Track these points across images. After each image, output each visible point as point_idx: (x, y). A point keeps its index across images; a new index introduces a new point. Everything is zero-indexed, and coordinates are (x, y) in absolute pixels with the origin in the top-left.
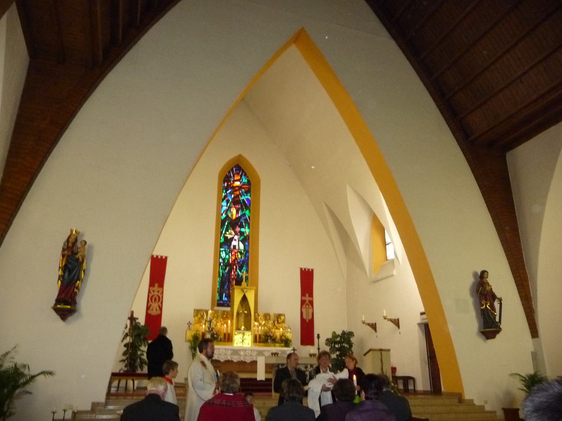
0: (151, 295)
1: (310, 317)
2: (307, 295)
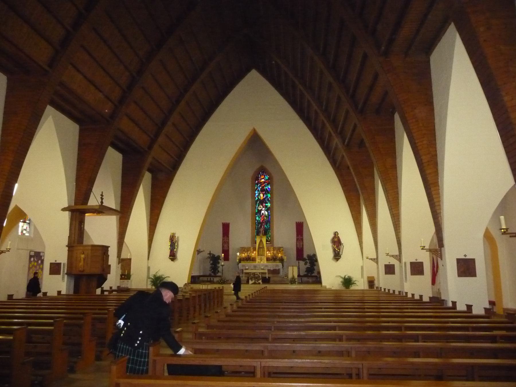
0: (224, 241)
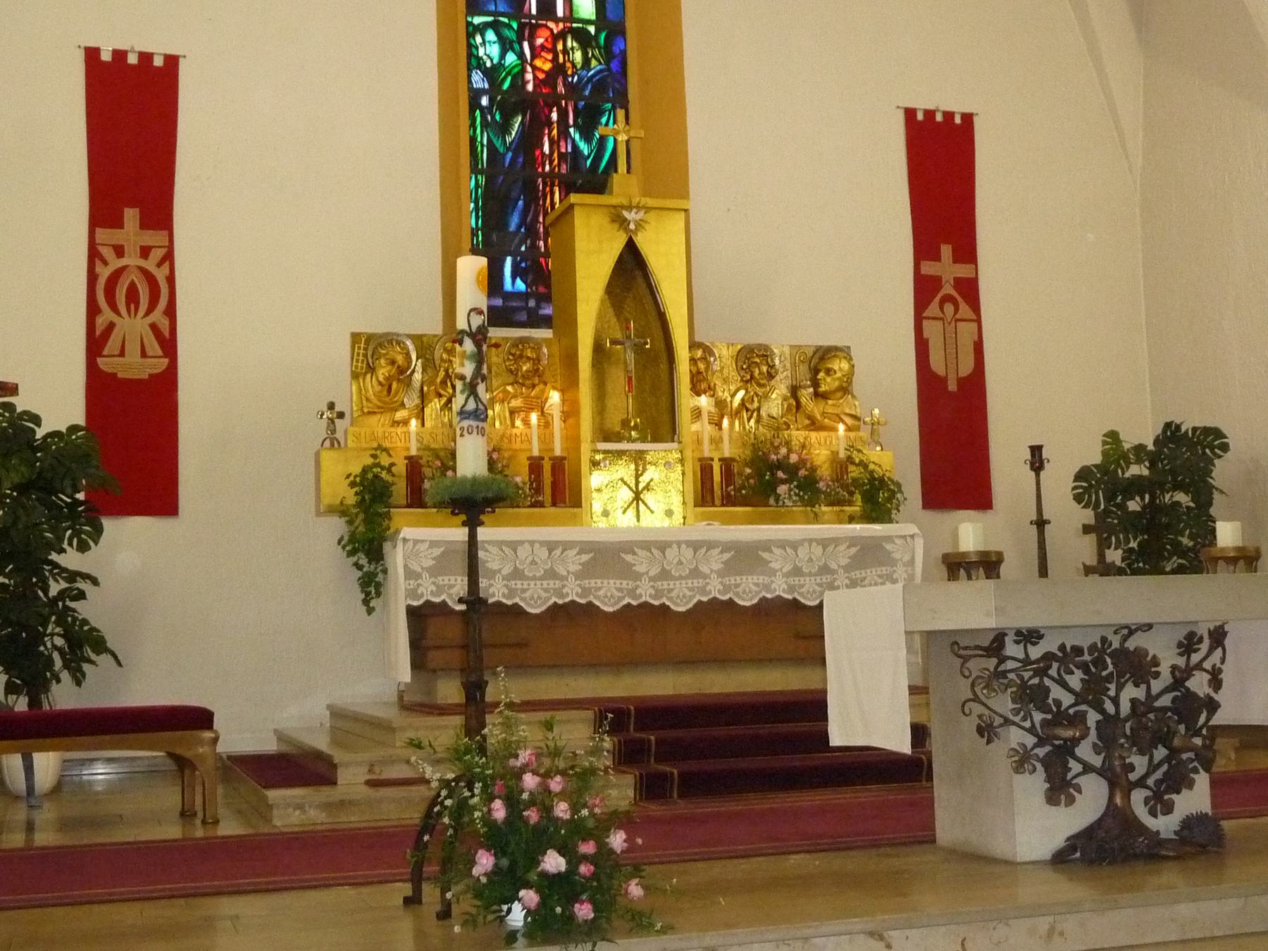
0: (104, 273)
1: (966, 367)
2: (946, 251)
